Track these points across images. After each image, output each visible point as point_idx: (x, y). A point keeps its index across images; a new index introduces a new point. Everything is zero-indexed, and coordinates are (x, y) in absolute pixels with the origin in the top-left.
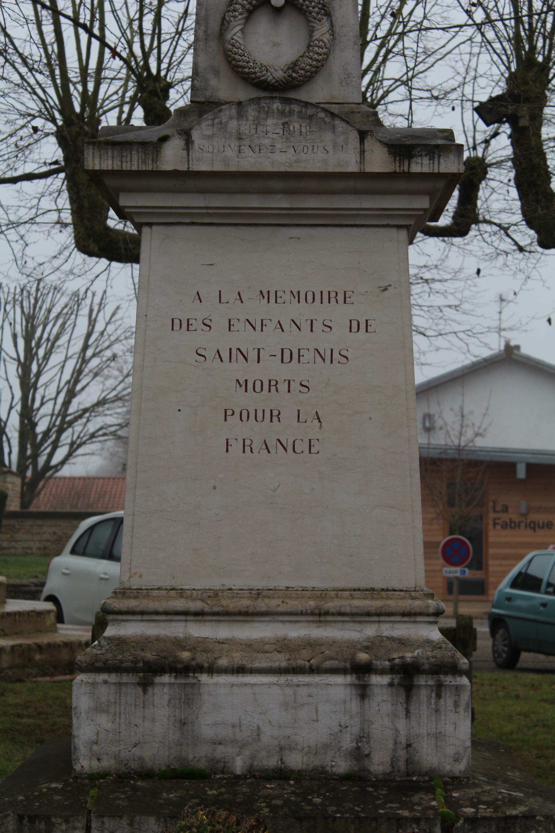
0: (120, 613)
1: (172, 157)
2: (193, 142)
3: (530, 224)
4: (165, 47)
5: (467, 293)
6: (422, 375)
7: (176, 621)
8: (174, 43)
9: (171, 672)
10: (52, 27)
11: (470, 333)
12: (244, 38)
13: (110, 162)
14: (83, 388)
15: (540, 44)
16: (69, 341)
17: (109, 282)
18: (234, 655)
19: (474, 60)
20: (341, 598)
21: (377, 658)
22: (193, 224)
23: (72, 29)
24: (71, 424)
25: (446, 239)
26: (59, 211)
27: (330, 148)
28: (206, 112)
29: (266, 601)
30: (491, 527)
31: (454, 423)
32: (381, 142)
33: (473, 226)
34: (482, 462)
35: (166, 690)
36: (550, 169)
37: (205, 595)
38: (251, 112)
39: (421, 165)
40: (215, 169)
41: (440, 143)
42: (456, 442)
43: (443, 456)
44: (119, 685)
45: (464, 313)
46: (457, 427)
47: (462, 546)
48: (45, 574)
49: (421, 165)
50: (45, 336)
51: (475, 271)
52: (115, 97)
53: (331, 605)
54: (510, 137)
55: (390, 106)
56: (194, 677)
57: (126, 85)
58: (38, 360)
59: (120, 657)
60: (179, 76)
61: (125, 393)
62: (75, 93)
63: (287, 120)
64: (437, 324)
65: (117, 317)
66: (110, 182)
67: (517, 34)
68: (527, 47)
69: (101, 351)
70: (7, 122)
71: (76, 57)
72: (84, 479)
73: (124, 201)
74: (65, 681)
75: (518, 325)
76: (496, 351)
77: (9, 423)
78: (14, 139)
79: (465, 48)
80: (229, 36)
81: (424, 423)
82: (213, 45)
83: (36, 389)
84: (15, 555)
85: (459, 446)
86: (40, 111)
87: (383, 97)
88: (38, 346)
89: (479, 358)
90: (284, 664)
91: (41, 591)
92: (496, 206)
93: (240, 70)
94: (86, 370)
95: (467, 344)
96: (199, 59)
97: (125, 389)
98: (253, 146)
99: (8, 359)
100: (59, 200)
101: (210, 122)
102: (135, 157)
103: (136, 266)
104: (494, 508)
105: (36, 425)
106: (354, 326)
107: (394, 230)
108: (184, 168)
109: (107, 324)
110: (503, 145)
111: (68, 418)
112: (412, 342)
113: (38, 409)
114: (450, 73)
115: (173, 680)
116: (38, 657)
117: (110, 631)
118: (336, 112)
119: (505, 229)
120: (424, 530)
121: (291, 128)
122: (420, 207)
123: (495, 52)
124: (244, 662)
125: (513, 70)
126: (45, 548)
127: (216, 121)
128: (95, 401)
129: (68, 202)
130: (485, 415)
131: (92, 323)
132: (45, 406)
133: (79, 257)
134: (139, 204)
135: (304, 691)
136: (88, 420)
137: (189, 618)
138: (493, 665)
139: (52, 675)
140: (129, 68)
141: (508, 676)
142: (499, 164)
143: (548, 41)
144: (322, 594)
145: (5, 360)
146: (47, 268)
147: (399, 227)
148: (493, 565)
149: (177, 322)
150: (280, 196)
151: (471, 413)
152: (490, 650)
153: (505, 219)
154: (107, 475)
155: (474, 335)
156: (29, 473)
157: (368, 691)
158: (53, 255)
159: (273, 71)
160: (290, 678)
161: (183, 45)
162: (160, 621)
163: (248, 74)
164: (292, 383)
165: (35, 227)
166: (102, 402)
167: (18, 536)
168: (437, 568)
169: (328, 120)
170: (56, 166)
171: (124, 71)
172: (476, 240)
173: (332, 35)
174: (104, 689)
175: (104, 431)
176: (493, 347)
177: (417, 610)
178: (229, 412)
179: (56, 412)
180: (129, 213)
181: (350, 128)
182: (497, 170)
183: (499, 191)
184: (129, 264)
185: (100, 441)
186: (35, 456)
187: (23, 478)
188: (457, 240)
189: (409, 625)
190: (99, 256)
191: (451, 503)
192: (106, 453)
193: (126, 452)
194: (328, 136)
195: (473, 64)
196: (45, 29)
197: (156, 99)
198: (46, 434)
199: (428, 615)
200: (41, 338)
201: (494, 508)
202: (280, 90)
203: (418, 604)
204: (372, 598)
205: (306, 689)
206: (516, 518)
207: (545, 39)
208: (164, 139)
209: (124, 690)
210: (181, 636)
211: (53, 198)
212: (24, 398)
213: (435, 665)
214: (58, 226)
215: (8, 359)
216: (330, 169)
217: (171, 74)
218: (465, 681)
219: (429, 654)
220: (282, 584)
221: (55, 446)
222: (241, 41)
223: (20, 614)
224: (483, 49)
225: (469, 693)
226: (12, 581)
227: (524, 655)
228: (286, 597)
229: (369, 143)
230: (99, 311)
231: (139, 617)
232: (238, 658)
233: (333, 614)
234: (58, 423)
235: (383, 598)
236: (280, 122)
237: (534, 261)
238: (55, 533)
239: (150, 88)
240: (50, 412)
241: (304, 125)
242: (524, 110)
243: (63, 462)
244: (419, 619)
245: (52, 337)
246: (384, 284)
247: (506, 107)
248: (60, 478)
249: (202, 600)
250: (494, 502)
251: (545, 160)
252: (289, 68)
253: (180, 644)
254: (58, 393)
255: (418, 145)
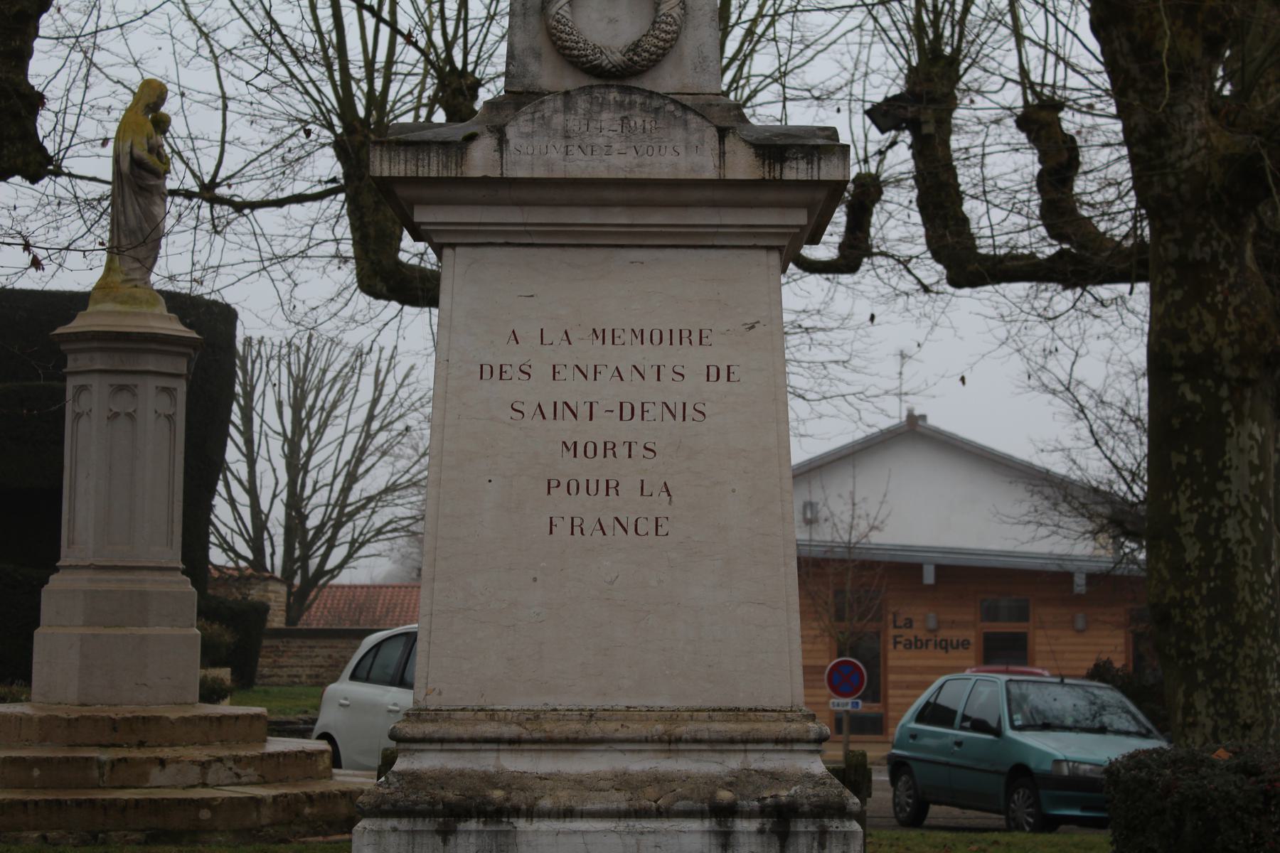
0: (413, 740)
1: (480, 160)
2: (507, 141)
3: (937, 257)
4: (472, 36)
5: (857, 345)
6: (800, 452)
7: (486, 750)
8: (484, 30)
9: (478, 817)
10: (329, 12)
11: (862, 396)
12: (572, 13)
13: (403, 167)
14: (367, 471)
15: (947, 33)
16: (349, 411)
17: (401, 332)
18: (560, 794)
19: (865, 52)
20: (697, 720)
21: (743, 797)
22: (507, 244)
23: (355, 14)
24: (351, 516)
25: (830, 276)
26: (337, 241)
27: (681, 150)
28: (525, 104)
29: (601, 724)
30: (891, 646)
31: (842, 513)
32: (745, 141)
33: (865, 260)
34: (879, 563)
35: (472, 840)
36: (962, 188)
37: (523, 718)
38: (582, 103)
39: (796, 171)
40: (536, 175)
41: (824, 144)
42: (846, 538)
43: (829, 555)
44: (412, 833)
45: (854, 371)
46: (847, 518)
47: (854, 670)
48: (317, 708)
49: (796, 171)
50: (319, 404)
51: (868, 317)
52: (409, 98)
53: (683, 730)
54: (910, 147)
55: (759, 110)
56: (509, 823)
57: (423, 82)
58: (309, 435)
59: (413, 797)
60: (490, 71)
61: (420, 477)
62: (359, 94)
63: (626, 113)
64: (820, 385)
65: (411, 379)
66: (403, 192)
67: (918, 18)
68: (931, 36)
69: (391, 423)
70: (272, 130)
71: (360, 49)
72: (368, 587)
73: (421, 216)
74: (343, 841)
75: (923, 386)
76: (896, 421)
77: (271, 516)
78: (280, 151)
79: (853, 37)
80: (553, 11)
81: (804, 513)
82: (534, 21)
83: (306, 472)
84: (278, 685)
85: (849, 542)
86: (314, 116)
87: (749, 98)
88: (310, 416)
89: (875, 430)
90: (624, 806)
91: (312, 730)
92: (893, 235)
93: (567, 52)
94: (371, 448)
95: (859, 411)
96: (516, 39)
97: (420, 472)
98: (584, 146)
99: (270, 433)
100: (337, 228)
101: (529, 117)
102: (434, 161)
103: (435, 311)
104: (895, 622)
105: (307, 517)
106: (714, 374)
107: (763, 253)
108: (497, 174)
109: (401, 386)
110: (903, 158)
111: (348, 509)
112: (786, 404)
113: (310, 498)
114: (835, 69)
115: (481, 827)
116: (307, 810)
117: (400, 765)
118: (689, 104)
119: (904, 263)
120: (804, 651)
121: (632, 124)
122: (795, 223)
123: (891, 41)
124: (573, 803)
125: (914, 64)
126: (317, 676)
127: (537, 115)
128: (383, 487)
129: (349, 230)
130: (882, 503)
131: (379, 387)
132: (318, 494)
133: (362, 300)
134: (439, 220)
135: (649, 840)
136: (373, 512)
137: (502, 747)
138: (894, 821)
139: (326, 834)
140: (428, 61)
141: (913, 833)
142: (898, 182)
143: (957, 29)
144: (673, 716)
145: (266, 435)
146: (322, 315)
147: (769, 248)
148: (894, 695)
149: (487, 369)
150: (617, 210)
151: (865, 499)
152: (890, 804)
153: (904, 250)
154: (395, 582)
155: (867, 399)
156: (297, 581)
157: (731, 840)
158: (330, 297)
159: (608, 53)
160: (631, 823)
161: (497, 30)
162: (465, 750)
163: (578, 56)
164: (633, 446)
165: (306, 262)
166: (390, 489)
167: (284, 661)
168: (823, 700)
169: (678, 114)
170: (334, 185)
171: (421, 65)
172: (868, 278)
173: (683, 9)
174: (392, 839)
175: (394, 525)
176: (891, 414)
177: (795, 736)
178: (554, 483)
179: (332, 501)
180: (426, 231)
181: (706, 124)
182: (894, 190)
183: (898, 217)
184: (427, 309)
185: (388, 539)
186: (305, 558)
187: (290, 586)
188: (845, 278)
189: (783, 756)
190: (389, 299)
191: (839, 616)
192: (396, 555)
193: (421, 554)
194: (679, 134)
195: (863, 57)
196: (320, 13)
197: (461, 99)
198: (320, 529)
199: (809, 742)
200: (313, 406)
201: (895, 622)
202: (619, 78)
203: (794, 728)
204: (737, 721)
205: (651, 838)
206: (922, 635)
207: (953, 27)
208: (471, 138)
209: (418, 839)
210: (492, 769)
211: (330, 224)
212: (292, 484)
213: (816, 806)
214: (336, 261)
215: (270, 433)
216: (682, 175)
217: (480, 68)
218: (855, 826)
219: (810, 791)
220: (622, 703)
221: (331, 544)
222: (568, 16)
223: (285, 755)
224: (876, 39)
225: (861, 842)
226: (274, 718)
227: (934, 810)
228: (626, 719)
229: (730, 142)
230: (388, 372)
231: (438, 746)
232: (564, 798)
233: (687, 741)
234: (334, 515)
235: (750, 720)
236: (618, 116)
237: (943, 305)
238: (330, 657)
239: (454, 86)
240: (325, 501)
241: (648, 120)
242: (928, 115)
243: (341, 566)
244: (796, 747)
245: (327, 406)
246: (750, 320)
247: (905, 108)
248: (338, 587)
249: (519, 724)
250: (895, 615)
251: (955, 176)
252: (629, 50)
253: (489, 780)
254: (335, 477)
255: (792, 146)
